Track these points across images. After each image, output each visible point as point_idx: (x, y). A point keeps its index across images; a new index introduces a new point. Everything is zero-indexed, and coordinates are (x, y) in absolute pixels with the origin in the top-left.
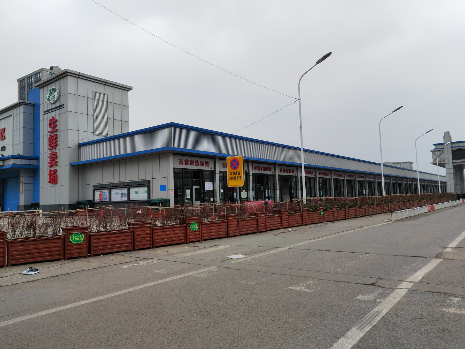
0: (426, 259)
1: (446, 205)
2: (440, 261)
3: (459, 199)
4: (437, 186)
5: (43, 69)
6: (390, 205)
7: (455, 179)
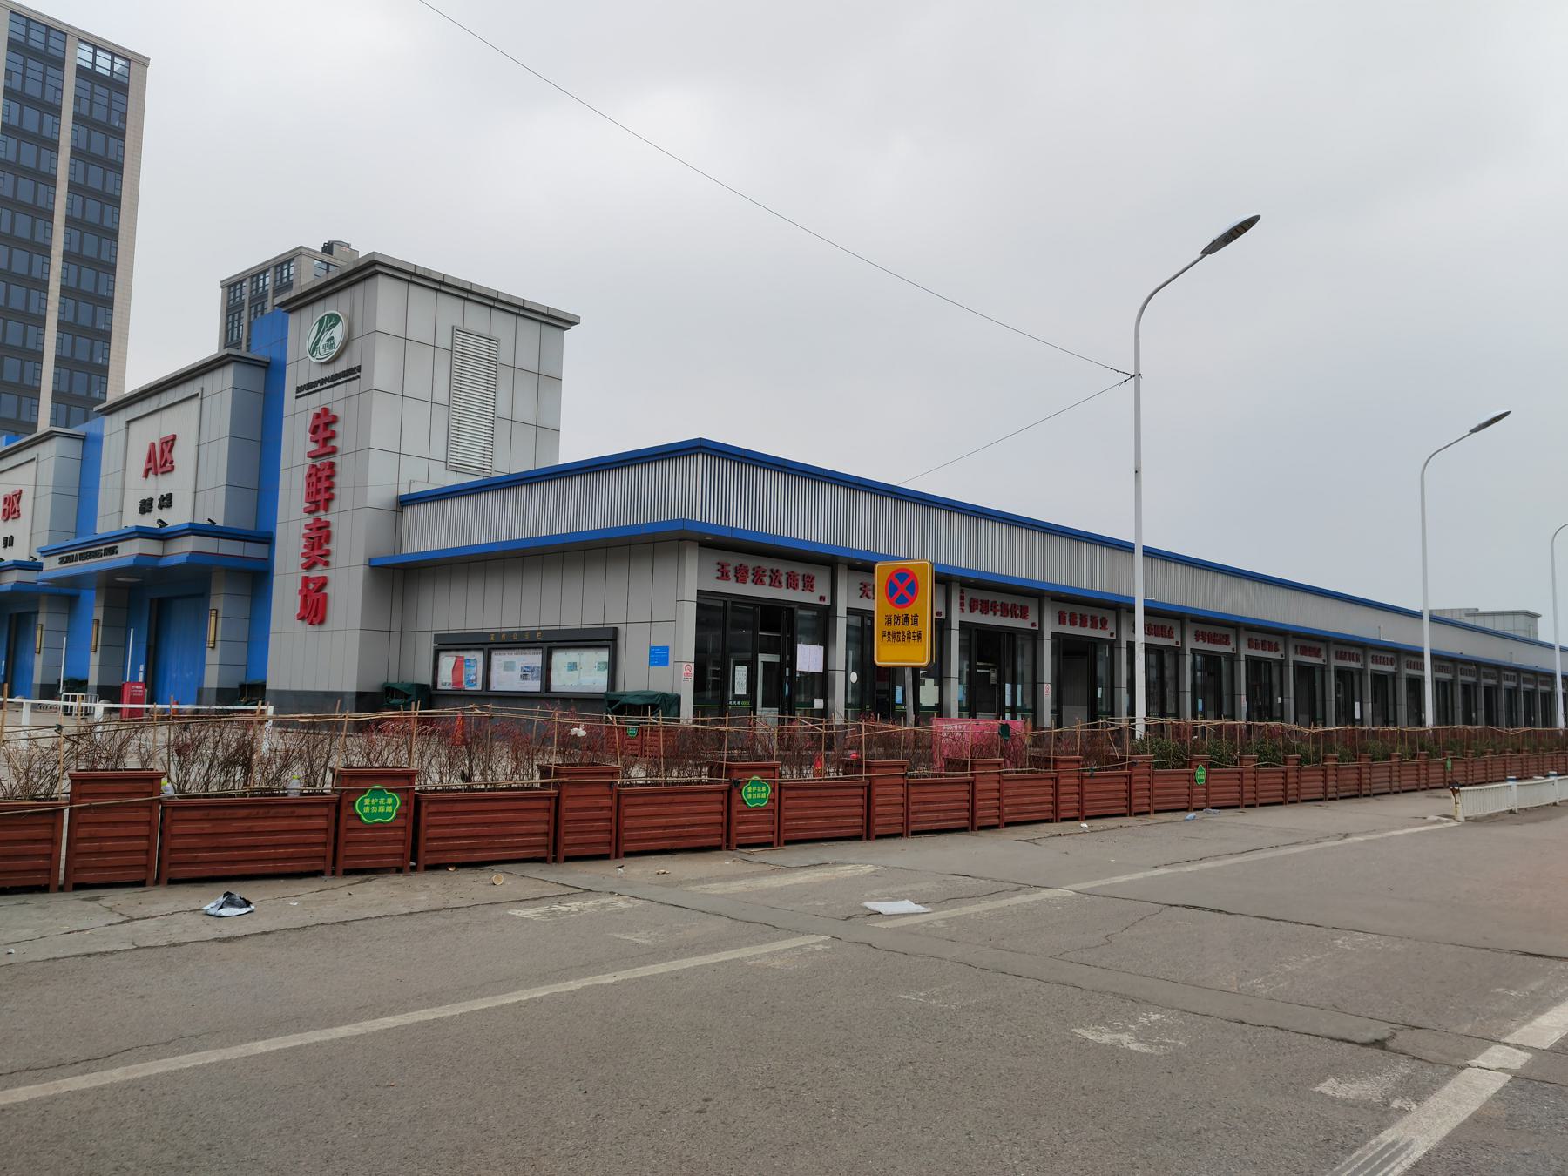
5: (303, 250)
6: (1449, 763)
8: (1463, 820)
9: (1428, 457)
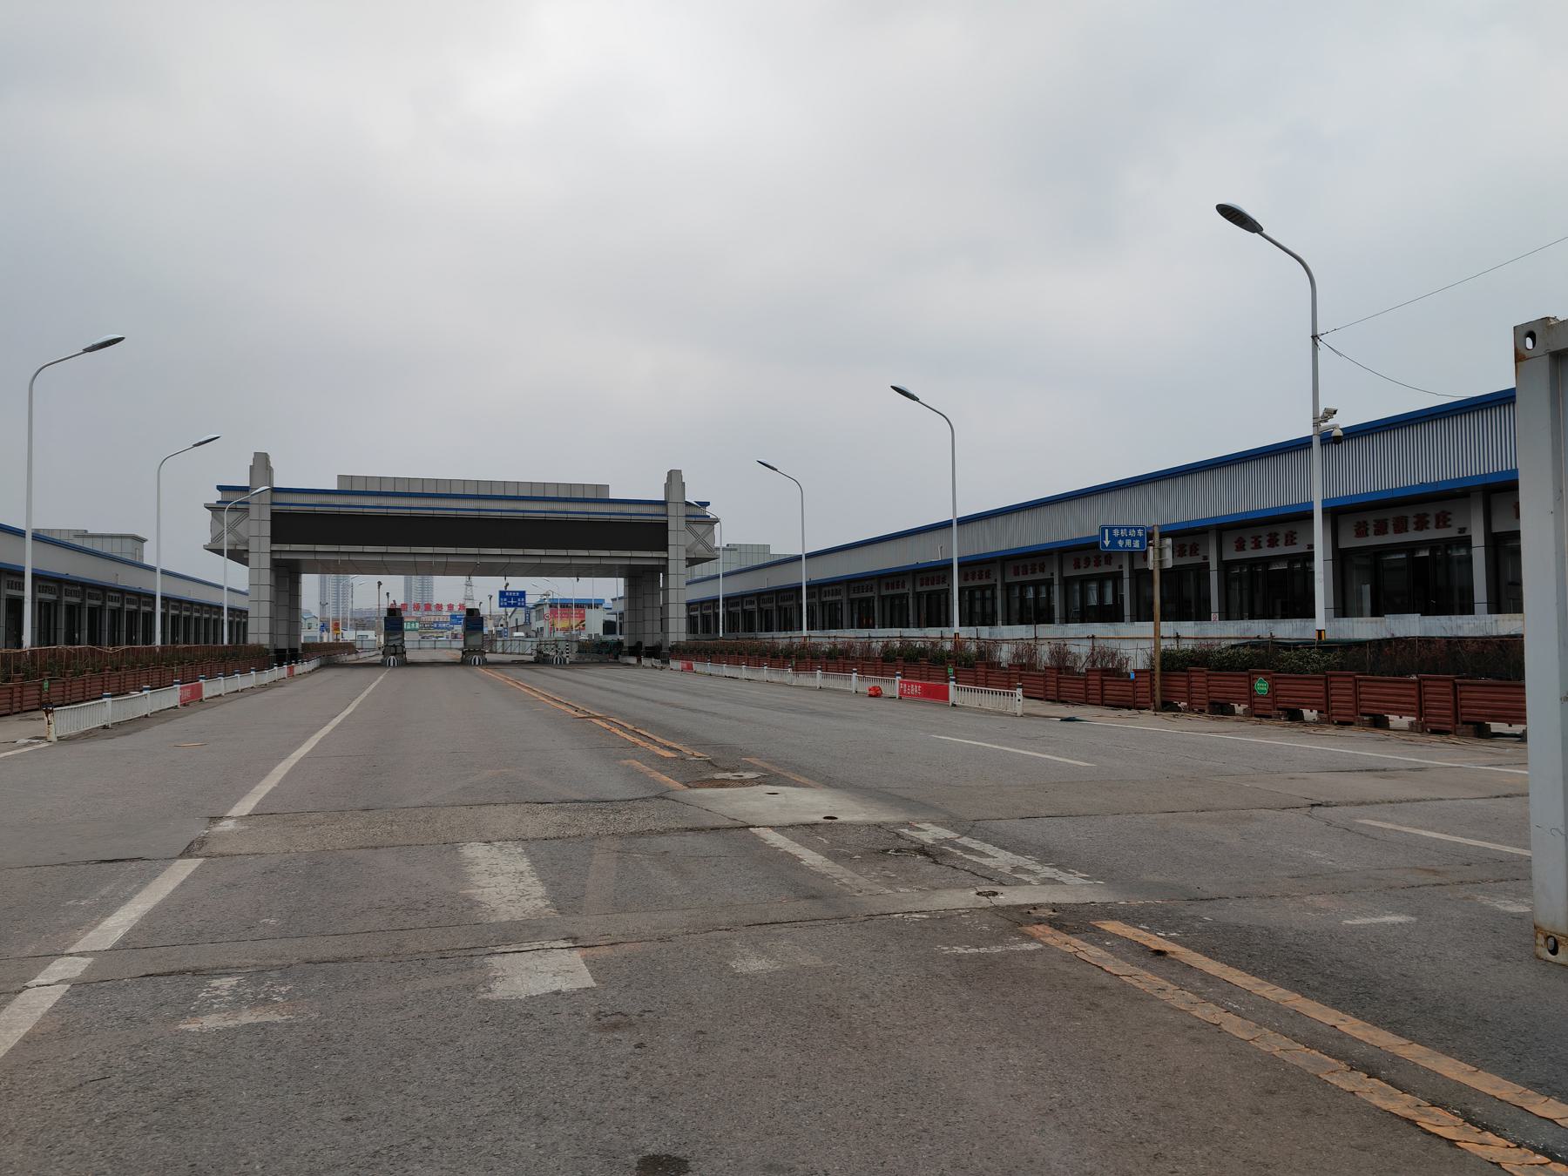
0: (143, 865)
1: (240, 681)
2: (196, 866)
3: (280, 665)
4: (218, 623)
6: (46, 684)
7: (275, 603)
8: (56, 740)
9: (39, 367)
